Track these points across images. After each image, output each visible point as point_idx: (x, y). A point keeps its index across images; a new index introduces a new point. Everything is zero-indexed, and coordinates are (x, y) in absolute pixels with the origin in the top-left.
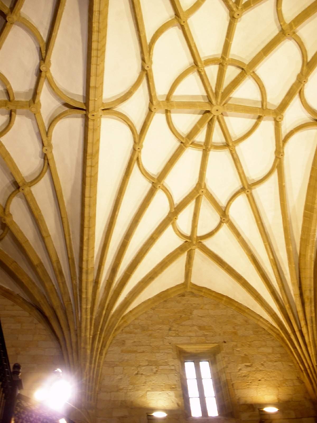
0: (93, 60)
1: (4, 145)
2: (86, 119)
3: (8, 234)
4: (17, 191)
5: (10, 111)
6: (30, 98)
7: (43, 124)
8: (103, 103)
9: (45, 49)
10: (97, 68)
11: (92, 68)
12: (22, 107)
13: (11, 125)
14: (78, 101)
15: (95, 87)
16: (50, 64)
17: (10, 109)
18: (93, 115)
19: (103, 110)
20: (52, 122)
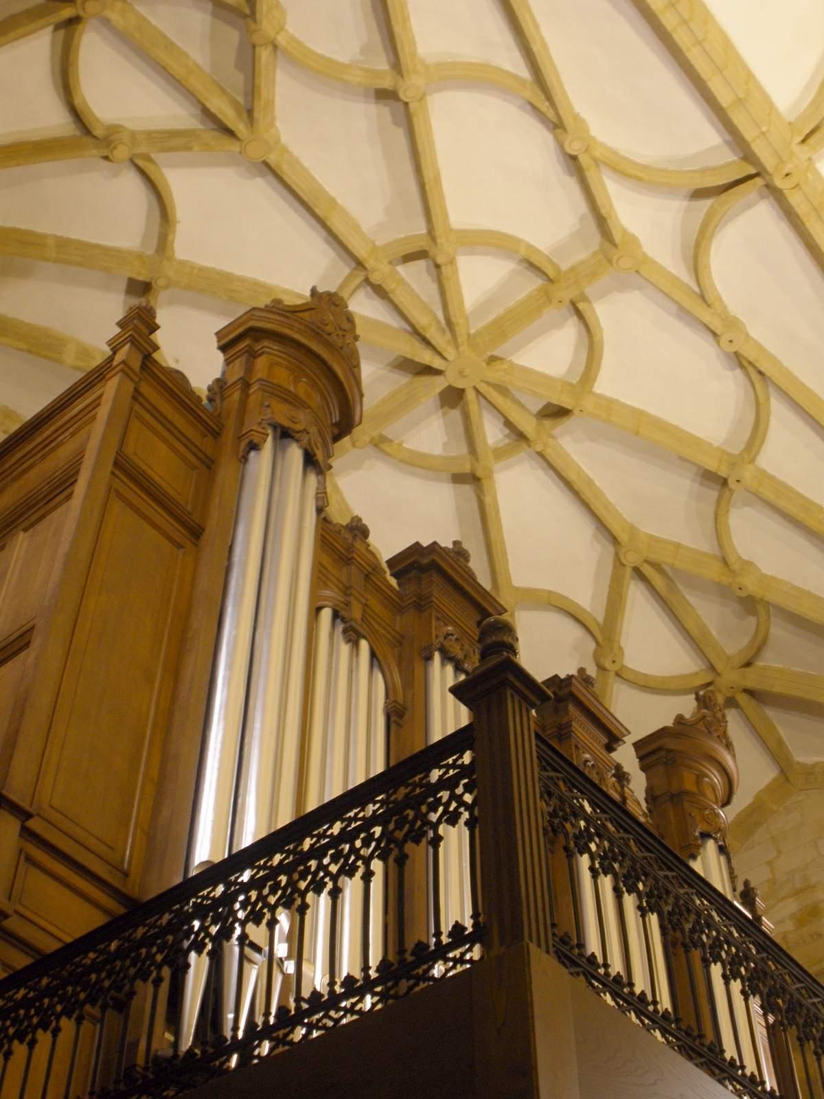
0: (682, 38)
1: (616, 397)
2: (777, 196)
3: (772, 618)
4: (727, 493)
5: (571, 307)
6: (596, 239)
7: (675, 280)
8: (790, 123)
9: (543, 97)
10: (705, 51)
11: (693, 62)
12: (593, 275)
13: (596, 339)
14: (722, 163)
15: (740, 101)
16: (583, 121)
17: (567, 302)
18: (787, 175)
19: (803, 141)
20: (696, 257)
